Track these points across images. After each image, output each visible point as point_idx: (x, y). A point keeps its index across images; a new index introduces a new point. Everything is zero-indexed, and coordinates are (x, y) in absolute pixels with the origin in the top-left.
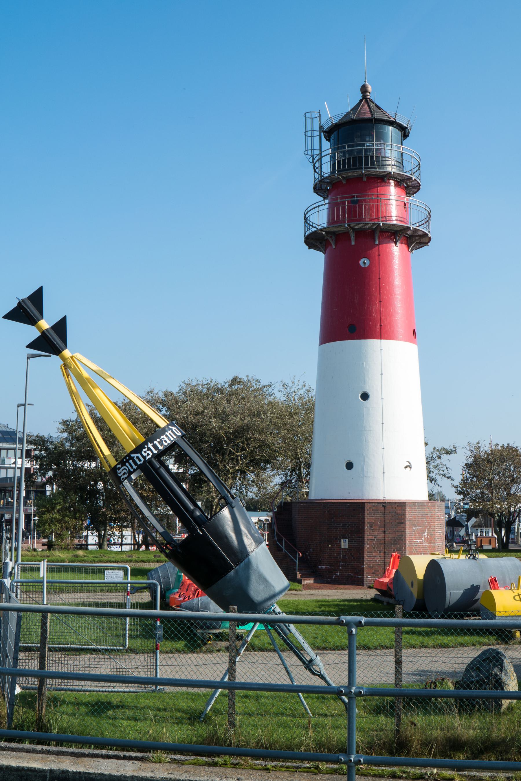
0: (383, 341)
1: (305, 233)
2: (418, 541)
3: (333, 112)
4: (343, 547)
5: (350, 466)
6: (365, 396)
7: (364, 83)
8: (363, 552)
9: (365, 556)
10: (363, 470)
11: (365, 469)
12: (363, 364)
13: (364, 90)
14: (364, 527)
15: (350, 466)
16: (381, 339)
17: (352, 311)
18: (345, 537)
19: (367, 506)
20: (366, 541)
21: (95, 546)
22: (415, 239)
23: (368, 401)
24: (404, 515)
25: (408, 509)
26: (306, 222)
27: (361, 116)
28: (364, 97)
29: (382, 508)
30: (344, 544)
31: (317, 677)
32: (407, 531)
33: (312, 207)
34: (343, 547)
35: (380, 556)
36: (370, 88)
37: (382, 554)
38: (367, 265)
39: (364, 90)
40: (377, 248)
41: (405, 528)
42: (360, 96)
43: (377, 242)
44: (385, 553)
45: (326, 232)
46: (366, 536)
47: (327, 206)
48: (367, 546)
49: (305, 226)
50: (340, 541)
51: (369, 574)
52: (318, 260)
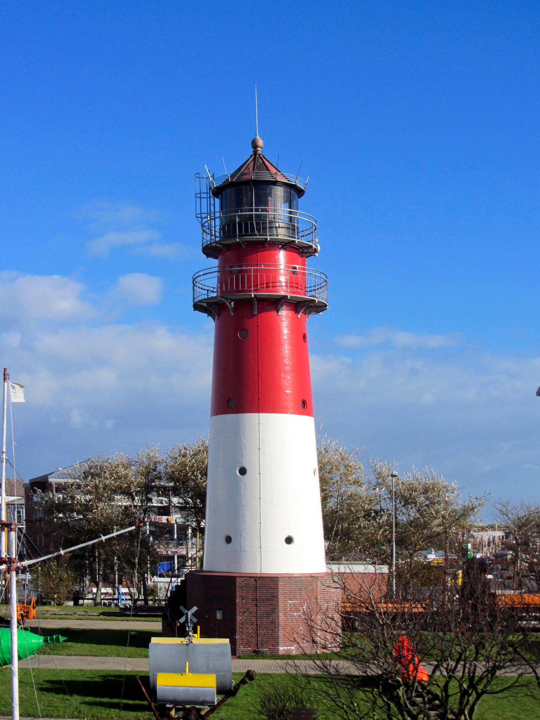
0: (263, 416)
1: (203, 244)
2: (295, 614)
3: (225, 171)
4: (218, 618)
5: (228, 540)
6: (243, 471)
8: (235, 624)
9: (238, 628)
10: (240, 545)
11: (242, 544)
12: (241, 438)
13: (255, 145)
14: (236, 600)
15: (228, 540)
16: (259, 413)
17: (241, 385)
18: (219, 609)
19: (238, 579)
20: (238, 612)
21: (91, 601)
22: (305, 306)
23: (246, 476)
24: (277, 588)
25: (281, 583)
27: (245, 177)
28: (255, 152)
29: (254, 582)
30: (219, 616)
31: (530, 697)
32: (281, 604)
34: (218, 618)
35: (252, 628)
36: (260, 142)
37: (254, 627)
40: (256, 316)
41: (278, 602)
42: (251, 151)
43: (256, 313)
44: (257, 625)
45: (207, 303)
46: (238, 608)
47: (216, 274)
48: (239, 618)
49: (194, 290)
50: (216, 613)
51: (242, 644)
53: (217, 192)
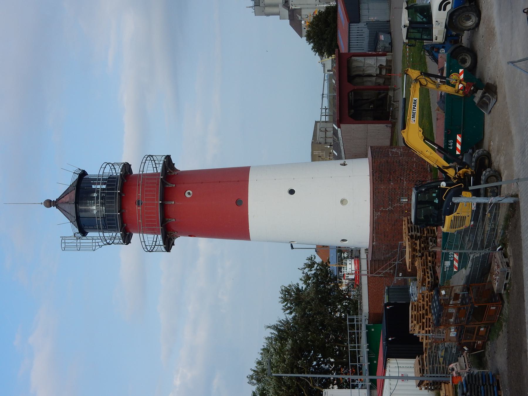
7: (43, 205)
13: (49, 203)
26: (152, 251)
33: (143, 243)
38: (191, 192)
39: (49, 203)
52: (181, 242)
53: (83, 232)
